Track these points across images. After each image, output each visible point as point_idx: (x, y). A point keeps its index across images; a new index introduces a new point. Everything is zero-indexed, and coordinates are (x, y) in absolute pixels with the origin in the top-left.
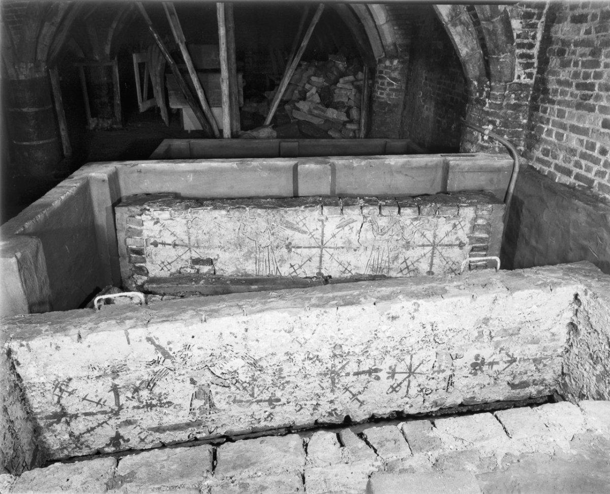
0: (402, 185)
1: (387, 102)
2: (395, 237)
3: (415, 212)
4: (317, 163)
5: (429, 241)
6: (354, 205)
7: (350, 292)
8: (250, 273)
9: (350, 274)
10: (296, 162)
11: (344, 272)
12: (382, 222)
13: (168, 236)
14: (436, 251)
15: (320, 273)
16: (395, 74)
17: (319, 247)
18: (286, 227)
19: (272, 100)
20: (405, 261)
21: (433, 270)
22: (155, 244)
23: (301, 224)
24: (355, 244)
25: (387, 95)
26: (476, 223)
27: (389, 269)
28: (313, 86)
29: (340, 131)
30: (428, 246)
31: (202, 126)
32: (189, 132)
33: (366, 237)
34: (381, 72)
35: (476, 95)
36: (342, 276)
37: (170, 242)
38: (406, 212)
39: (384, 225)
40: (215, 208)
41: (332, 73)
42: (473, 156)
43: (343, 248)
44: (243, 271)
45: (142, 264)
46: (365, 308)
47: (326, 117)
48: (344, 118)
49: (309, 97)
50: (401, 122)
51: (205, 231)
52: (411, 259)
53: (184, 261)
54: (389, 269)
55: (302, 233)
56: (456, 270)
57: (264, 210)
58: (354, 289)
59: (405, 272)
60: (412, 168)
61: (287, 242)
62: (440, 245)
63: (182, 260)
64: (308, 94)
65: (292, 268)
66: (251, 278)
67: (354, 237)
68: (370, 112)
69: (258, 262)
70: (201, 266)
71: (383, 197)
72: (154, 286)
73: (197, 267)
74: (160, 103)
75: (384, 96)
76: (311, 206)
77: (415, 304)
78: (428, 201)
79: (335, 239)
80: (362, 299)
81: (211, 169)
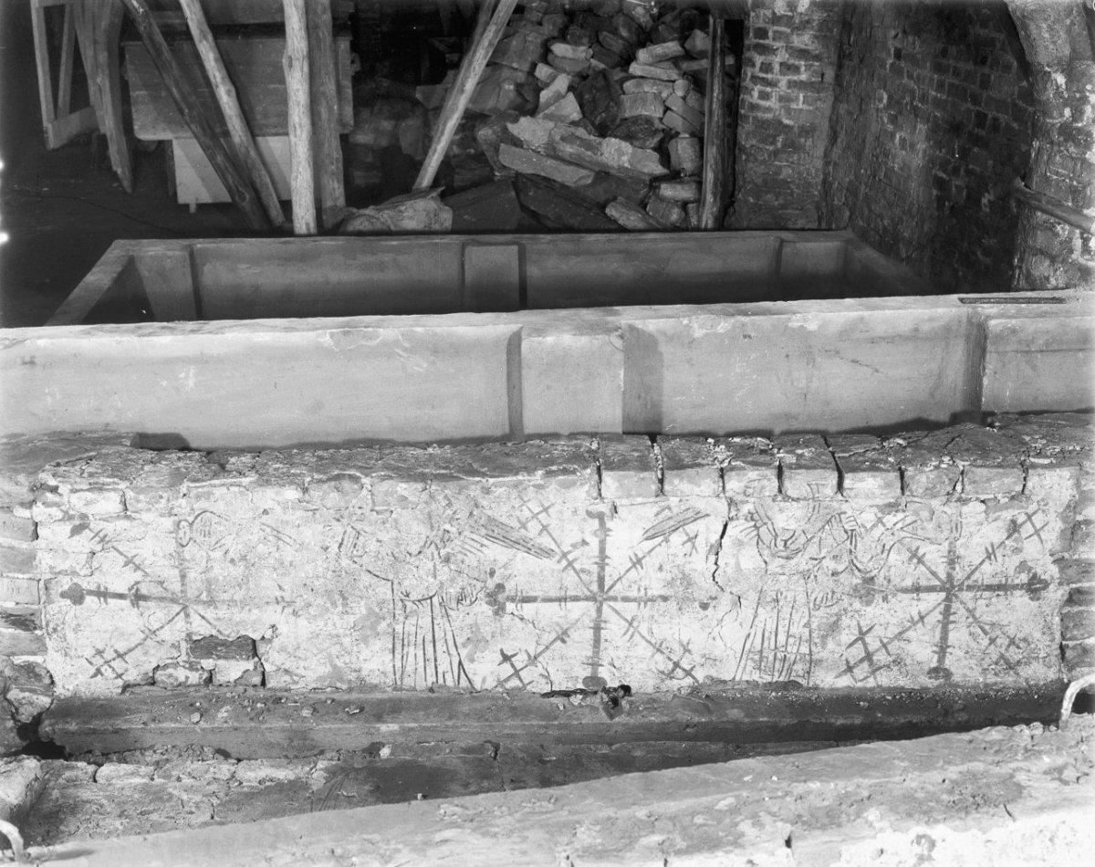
0: (849, 389)
1: (780, 123)
2: (829, 564)
3: (888, 485)
4: (581, 329)
5: (934, 574)
6: (700, 465)
7: (705, 800)
8: (375, 681)
9: (689, 681)
10: (514, 327)
11: (670, 676)
12: (788, 518)
13: (117, 569)
14: (955, 606)
15: (594, 680)
16: (804, 40)
17: (592, 598)
18: (487, 536)
19: (438, 110)
20: (862, 636)
21: (948, 663)
22: (76, 596)
23: (534, 528)
24: (705, 587)
25: (781, 99)
26: (1080, 518)
27: (813, 663)
28: (559, 70)
29: (643, 205)
30: (931, 589)
31: (232, 196)
32: (193, 209)
33: (738, 564)
34: (762, 33)
35: (1062, 115)
36: (664, 688)
37: (122, 589)
38: (859, 485)
39: (793, 527)
40: (265, 480)
41: (615, 32)
42: (1060, 301)
43: (665, 599)
44: (353, 676)
45: (32, 659)
46: (755, 859)
47: (598, 164)
48: (653, 167)
49: (548, 105)
50: (824, 181)
51: (231, 555)
52: (878, 631)
53: (167, 646)
54: (813, 663)
55: (537, 555)
56: (1019, 662)
57: (420, 486)
58: (719, 788)
59: (861, 671)
60: (873, 341)
61: (491, 584)
62: (970, 588)
63: (161, 643)
64: (545, 95)
65: (507, 666)
66: (379, 696)
67: (700, 565)
68: (731, 148)
69: (398, 647)
70: (221, 662)
71: (792, 437)
72: (73, 727)
73: (208, 663)
74: (108, 124)
75: (773, 103)
76: (565, 472)
77: (919, 838)
78: (930, 450)
79: (642, 572)
80: (746, 827)
81: (253, 352)
